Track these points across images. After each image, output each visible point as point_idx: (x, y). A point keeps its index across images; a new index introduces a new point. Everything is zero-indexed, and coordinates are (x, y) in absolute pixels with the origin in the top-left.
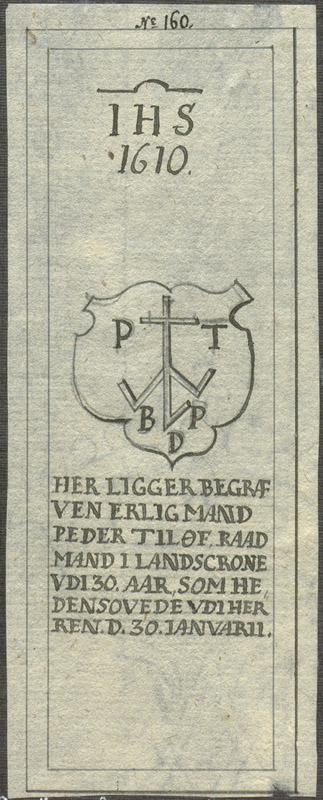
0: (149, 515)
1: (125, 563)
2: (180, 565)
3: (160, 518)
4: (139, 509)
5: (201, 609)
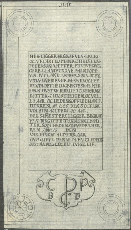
0: (93, 57)
1: (65, 97)
2: (48, 135)
3: (90, 107)
4: (91, 56)
5: (36, 140)
